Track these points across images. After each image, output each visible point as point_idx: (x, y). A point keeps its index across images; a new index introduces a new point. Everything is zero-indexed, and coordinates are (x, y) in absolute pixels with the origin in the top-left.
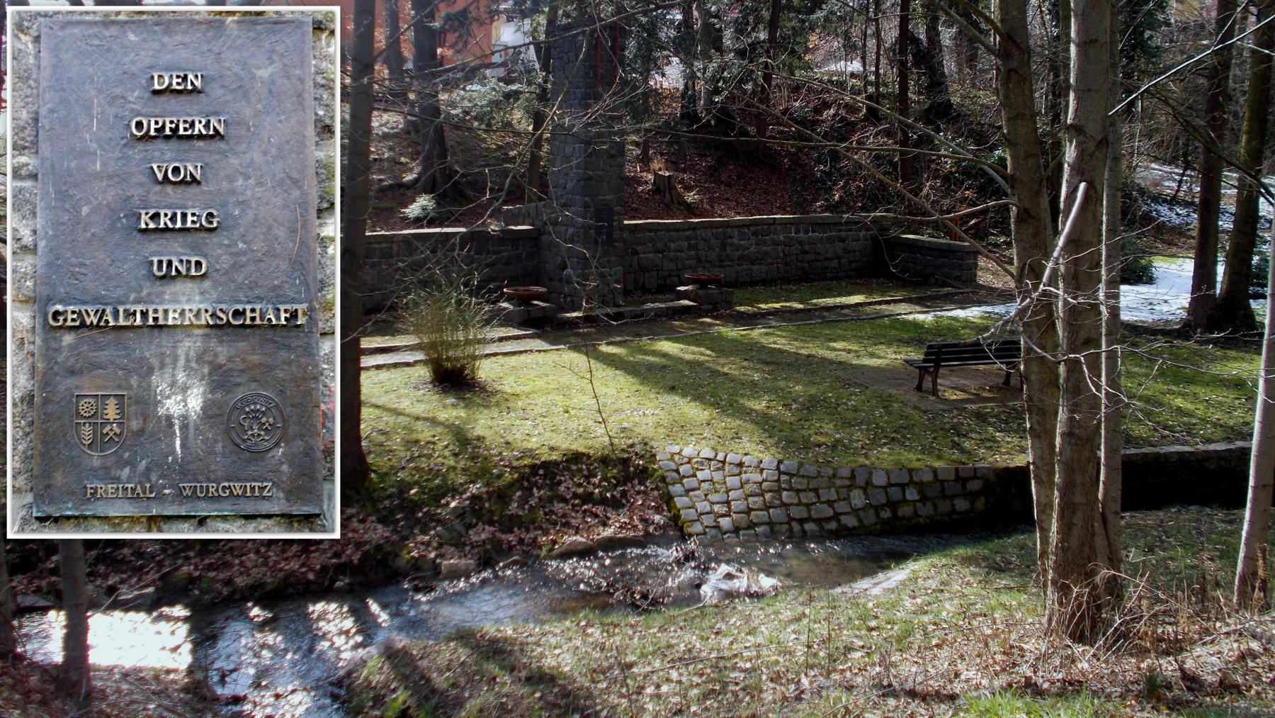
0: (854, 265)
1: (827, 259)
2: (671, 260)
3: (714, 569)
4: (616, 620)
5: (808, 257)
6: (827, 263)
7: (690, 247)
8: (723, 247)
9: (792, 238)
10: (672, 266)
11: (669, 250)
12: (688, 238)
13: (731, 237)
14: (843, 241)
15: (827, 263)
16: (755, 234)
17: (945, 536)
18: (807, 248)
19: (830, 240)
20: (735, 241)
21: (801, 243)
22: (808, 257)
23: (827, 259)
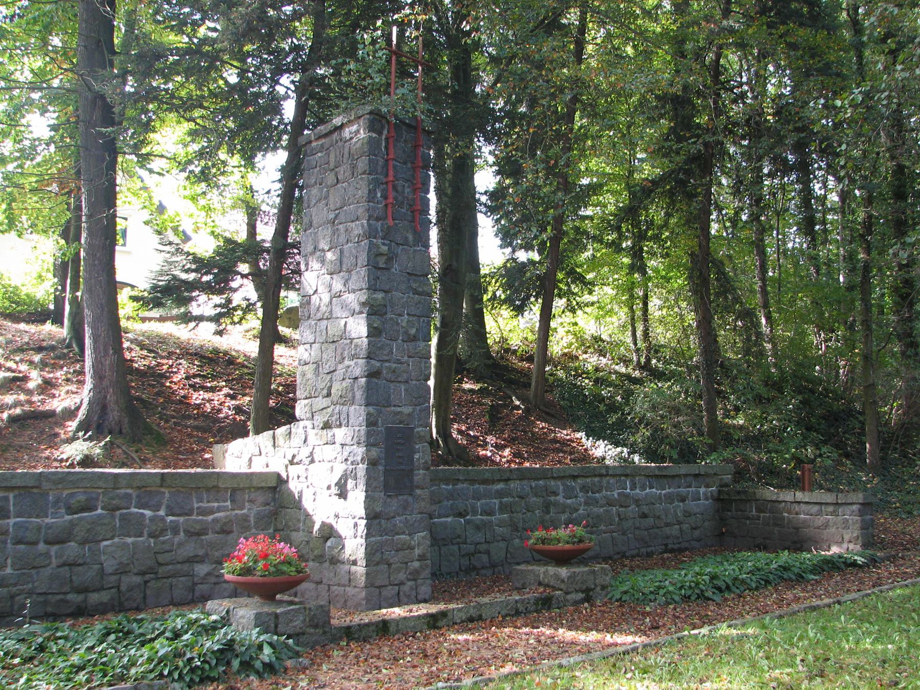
0: (697, 533)
1: (668, 525)
2: (478, 528)
3: (493, 227)
4: (567, 546)
5: (650, 521)
6: (667, 530)
7: (503, 508)
8: (547, 507)
9: (627, 496)
10: (479, 537)
11: (475, 513)
12: (500, 494)
13: (555, 494)
14: (683, 500)
15: (667, 530)
16: (584, 489)
17: (91, 394)
18: (645, 509)
19: (670, 498)
20: (560, 498)
21: (637, 502)
22: (650, 521)
23: (668, 525)
